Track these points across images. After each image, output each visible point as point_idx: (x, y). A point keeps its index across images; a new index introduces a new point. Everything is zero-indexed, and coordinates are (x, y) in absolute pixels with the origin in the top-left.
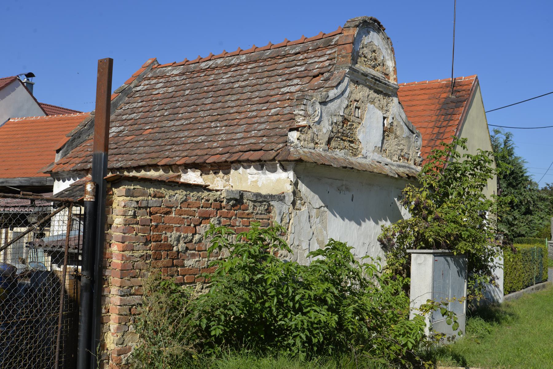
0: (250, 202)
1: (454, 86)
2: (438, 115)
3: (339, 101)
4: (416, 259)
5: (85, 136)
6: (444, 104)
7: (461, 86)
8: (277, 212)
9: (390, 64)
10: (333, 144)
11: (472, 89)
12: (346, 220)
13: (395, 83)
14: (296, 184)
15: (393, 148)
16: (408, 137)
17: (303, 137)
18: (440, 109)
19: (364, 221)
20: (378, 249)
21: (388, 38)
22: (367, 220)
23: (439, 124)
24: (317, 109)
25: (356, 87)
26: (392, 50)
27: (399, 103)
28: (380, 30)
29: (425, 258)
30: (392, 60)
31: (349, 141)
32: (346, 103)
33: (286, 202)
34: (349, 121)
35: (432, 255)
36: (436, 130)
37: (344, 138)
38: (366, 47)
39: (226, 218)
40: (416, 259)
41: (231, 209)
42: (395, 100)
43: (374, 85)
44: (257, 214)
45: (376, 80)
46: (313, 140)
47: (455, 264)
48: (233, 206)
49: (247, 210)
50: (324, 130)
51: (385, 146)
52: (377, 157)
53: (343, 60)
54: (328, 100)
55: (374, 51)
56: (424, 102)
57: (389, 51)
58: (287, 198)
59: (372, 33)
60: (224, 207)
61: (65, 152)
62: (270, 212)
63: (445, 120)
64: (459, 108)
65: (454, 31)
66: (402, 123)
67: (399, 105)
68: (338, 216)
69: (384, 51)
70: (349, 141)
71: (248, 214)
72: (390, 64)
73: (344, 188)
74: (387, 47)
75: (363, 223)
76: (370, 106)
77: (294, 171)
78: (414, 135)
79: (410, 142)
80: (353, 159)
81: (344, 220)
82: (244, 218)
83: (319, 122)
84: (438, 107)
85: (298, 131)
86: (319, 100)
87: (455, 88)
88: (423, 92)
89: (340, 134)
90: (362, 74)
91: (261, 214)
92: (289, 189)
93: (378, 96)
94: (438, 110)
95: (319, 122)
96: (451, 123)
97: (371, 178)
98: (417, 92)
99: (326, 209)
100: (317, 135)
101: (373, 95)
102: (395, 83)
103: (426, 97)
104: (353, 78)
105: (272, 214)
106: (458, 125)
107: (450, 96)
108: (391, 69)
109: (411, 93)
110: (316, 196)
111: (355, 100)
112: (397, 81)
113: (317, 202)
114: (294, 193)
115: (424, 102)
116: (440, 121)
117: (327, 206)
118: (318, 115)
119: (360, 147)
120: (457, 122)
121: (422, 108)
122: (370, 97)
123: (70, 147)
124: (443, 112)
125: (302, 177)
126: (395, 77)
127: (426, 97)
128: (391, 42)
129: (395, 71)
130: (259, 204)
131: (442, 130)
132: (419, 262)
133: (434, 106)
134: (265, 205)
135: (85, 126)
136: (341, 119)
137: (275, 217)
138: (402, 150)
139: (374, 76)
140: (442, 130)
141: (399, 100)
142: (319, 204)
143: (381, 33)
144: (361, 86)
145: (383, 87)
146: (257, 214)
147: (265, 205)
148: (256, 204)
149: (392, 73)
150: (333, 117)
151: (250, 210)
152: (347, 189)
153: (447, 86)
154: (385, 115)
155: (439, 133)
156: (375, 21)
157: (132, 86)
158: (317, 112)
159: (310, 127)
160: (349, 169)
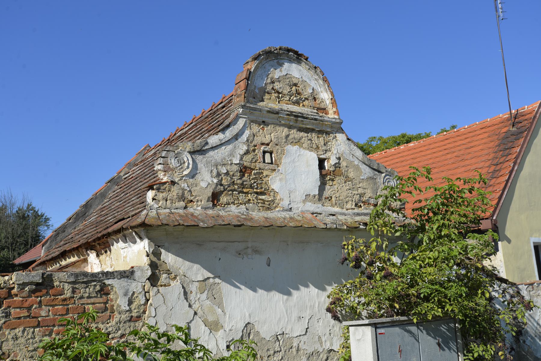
0: (66, 284)
1: (515, 119)
2: (496, 152)
3: (230, 147)
4: (354, 334)
5: (71, 229)
6: (504, 138)
7: (523, 116)
8: (120, 292)
9: (325, 96)
10: (224, 199)
11: (535, 117)
12: (260, 291)
13: (336, 117)
14: (157, 254)
15: (345, 194)
16: (372, 178)
17: (161, 196)
18: (499, 145)
19: (298, 289)
20: (329, 322)
21: (315, 68)
22: (302, 288)
23: (495, 162)
24: (185, 159)
25: (263, 129)
26: (325, 80)
27: (348, 139)
28: (301, 60)
29: (363, 331)
30: (326, 91)
31: (257, 193)
32: (245, 148)
33: (137, 278)
34: (253, 169)
35: (370, 327)
36: (493, 168)
37: (245, 190)
38: (279, 81)
39: (20, 308)
40: (354, 334)
41: (29, 296)
42: (341, 137)
43: (296, 123)
44: (82, 297)
45: (295, 116)
46: (182, 198)
47: (428, 334)
48: (33, 292)
49: (61, 295)
50: (203, 184)
51: (326, 194)
52: (311, 207)
53: (238, 99)
54: (206, 147)
55: (295, 85)
56: (484, 141)
57: (321, 82)
58: (137, 274)
59: (286, 64)
60: (16, 295)
61: (48, 248)
62: (108, 294)
63: (502, 156)
64: (518, 139)
65: (504, 60)
66: (356, 162)
67: (347, 142)
68: (242, 287)
69: (313, 84)
70: (257, 193)
71: (65, 300)
72: (325, 96)
73: (250, 251)
74: (317, 77)
75: (294, 292)
76: (293, 149)
77: (149, 239)
78: (383, 175)
79: (375, 183)
80: (270, 214)
81: (255, 291)
82: (56, 305)
83: (192, 175)
84: (497, 143)
85: (153, 189)
86: (188, 149)
87: (517, 120)
88: (484, 130)
89: (236, 187)
90: (269, 112)
91: (89, 297)
92: (145, 261)
93: (306, 135)
94: (496, 146)
95: (192, 175)
96: (509, 157)
97: (301, 235)
98: (478, 132)
99: (217, 280)
100: (190, 191)
101: (294, 134)
102: (336, 117)
103: (486, 135)
104: (253, 118)
105: (111, 296)
106: (517, 158)
107: (511, 129)
108: (328, 102)
109: (471, 134)
110: (196, 266)
111: (263, 144)
112: (338, 114)
113: (197, 272)
114: (153, 266)
115: (484, 141)
116: (497, 158)
117: (219, 277)
118: (188, 167)
119: (278, 198)
120: (514, 156)
121: (480, 147)
122: (290, 137)
123: (54, 242)
124: (502, 147)
125: (166, 244)
126: (335, 109)
127: (486, 135)
128: (321, 71)
129: (334, 102)
130: (83, 285)
131: (498, 168)
132: (358, 338)
133: (493, 143)
134: (95, 286)
135: (70, 219)
136: (235, 168)
137: (117, 299)
138: (361, 195)
139: (292, 112)
140: (498, 168)
141: (346, 135)
142: (203, 275)
143: (303, 64)
144: (272, 126)
145: (313, 124)
146: (82, 297)
147: (95, 286)
148: (77, 286)
149: (330, 106)
150: (219, 167)
151: (68, 294)
152: (256, 251)
153: (508, 120)
154: (322, 157)
155: (495, 171)
156: (289, 50)
157: (122, 174)
158: (186, 164)
159: (173, 183)
160: (272, 229)
